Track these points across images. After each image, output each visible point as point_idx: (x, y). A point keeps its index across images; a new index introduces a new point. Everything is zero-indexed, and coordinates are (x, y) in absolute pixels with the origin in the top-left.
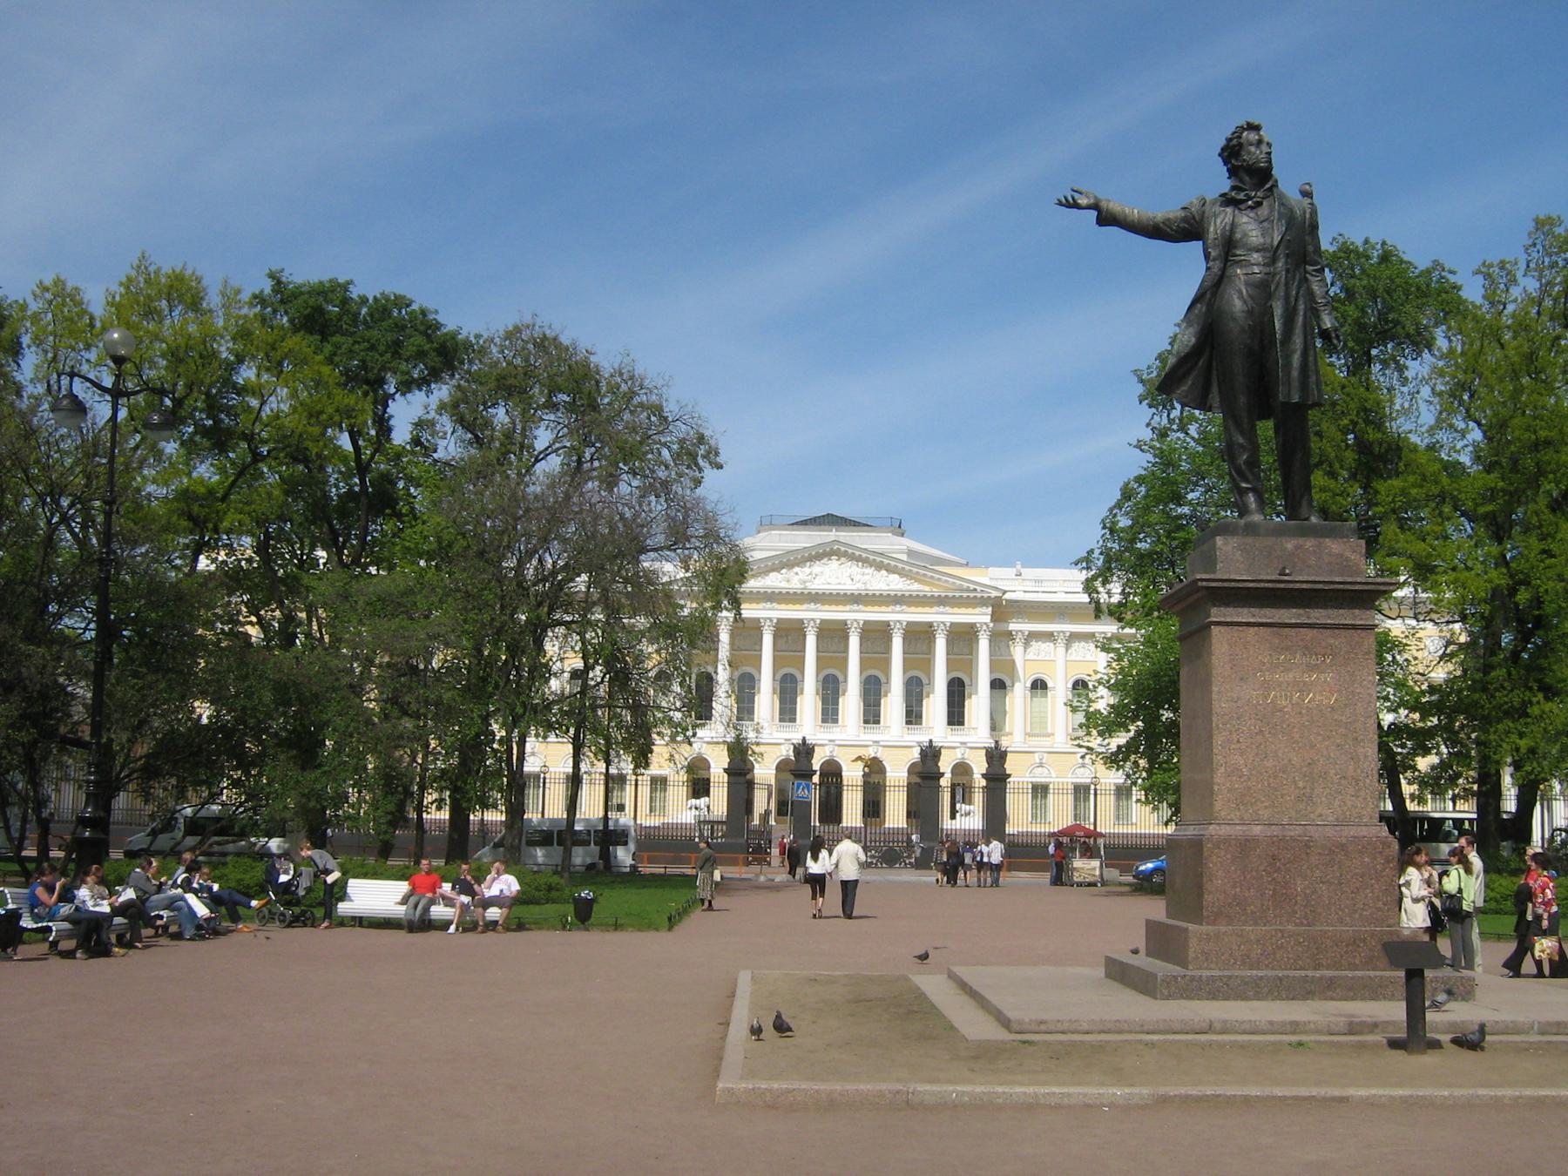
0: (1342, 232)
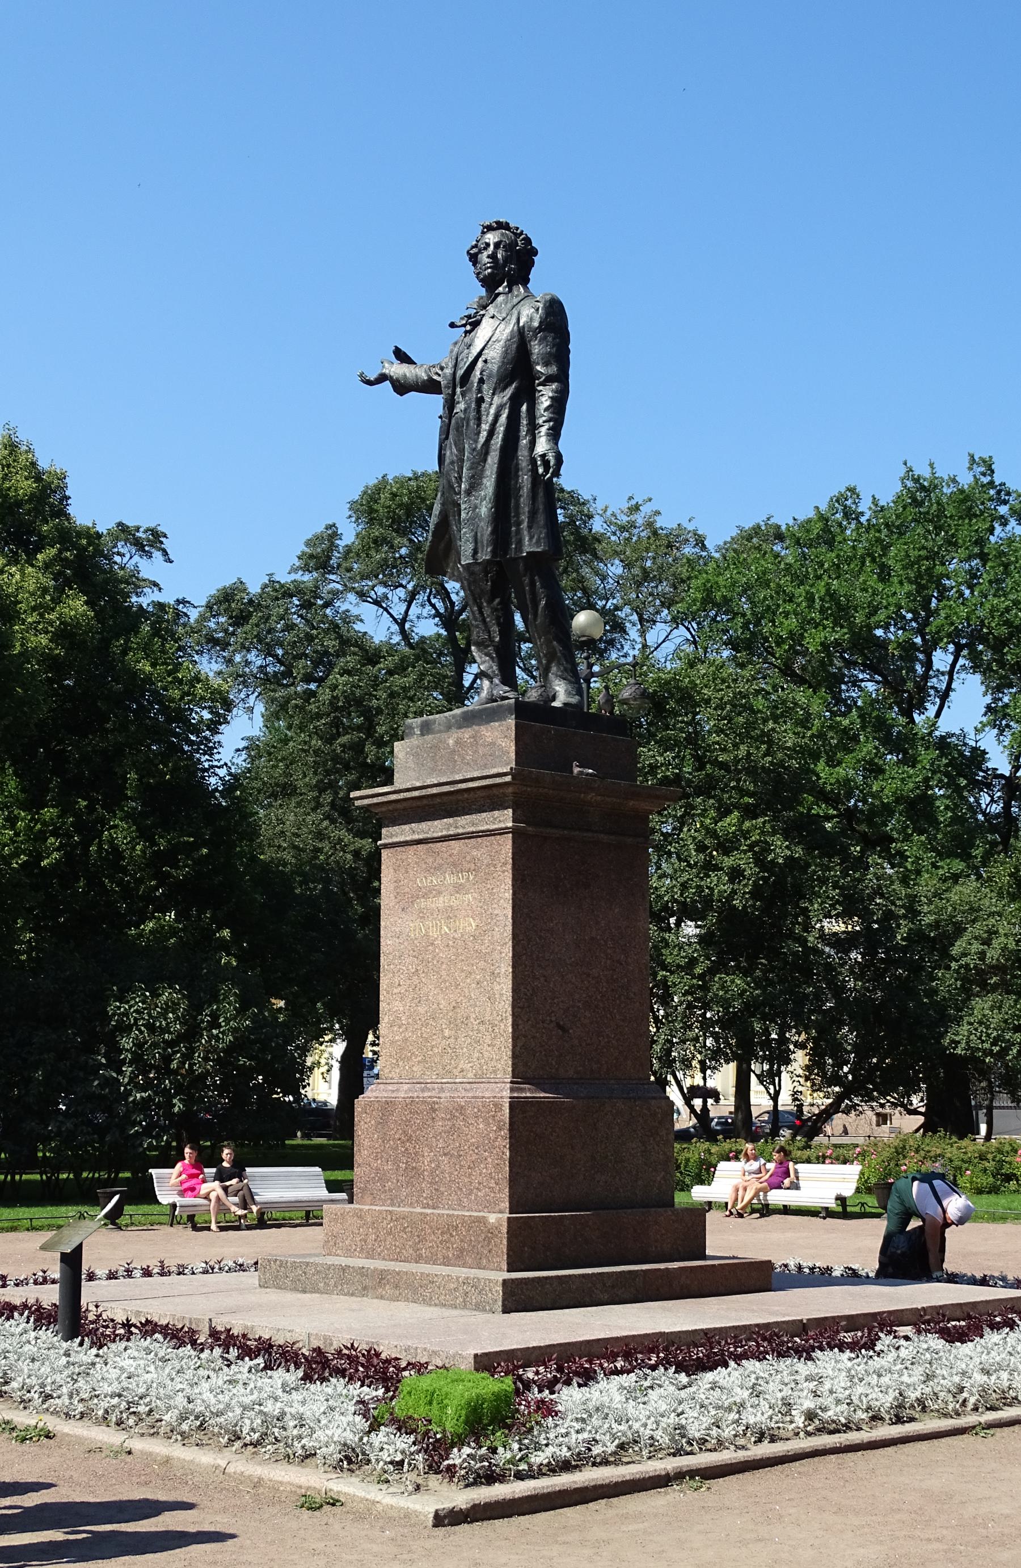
0: (454, 341)
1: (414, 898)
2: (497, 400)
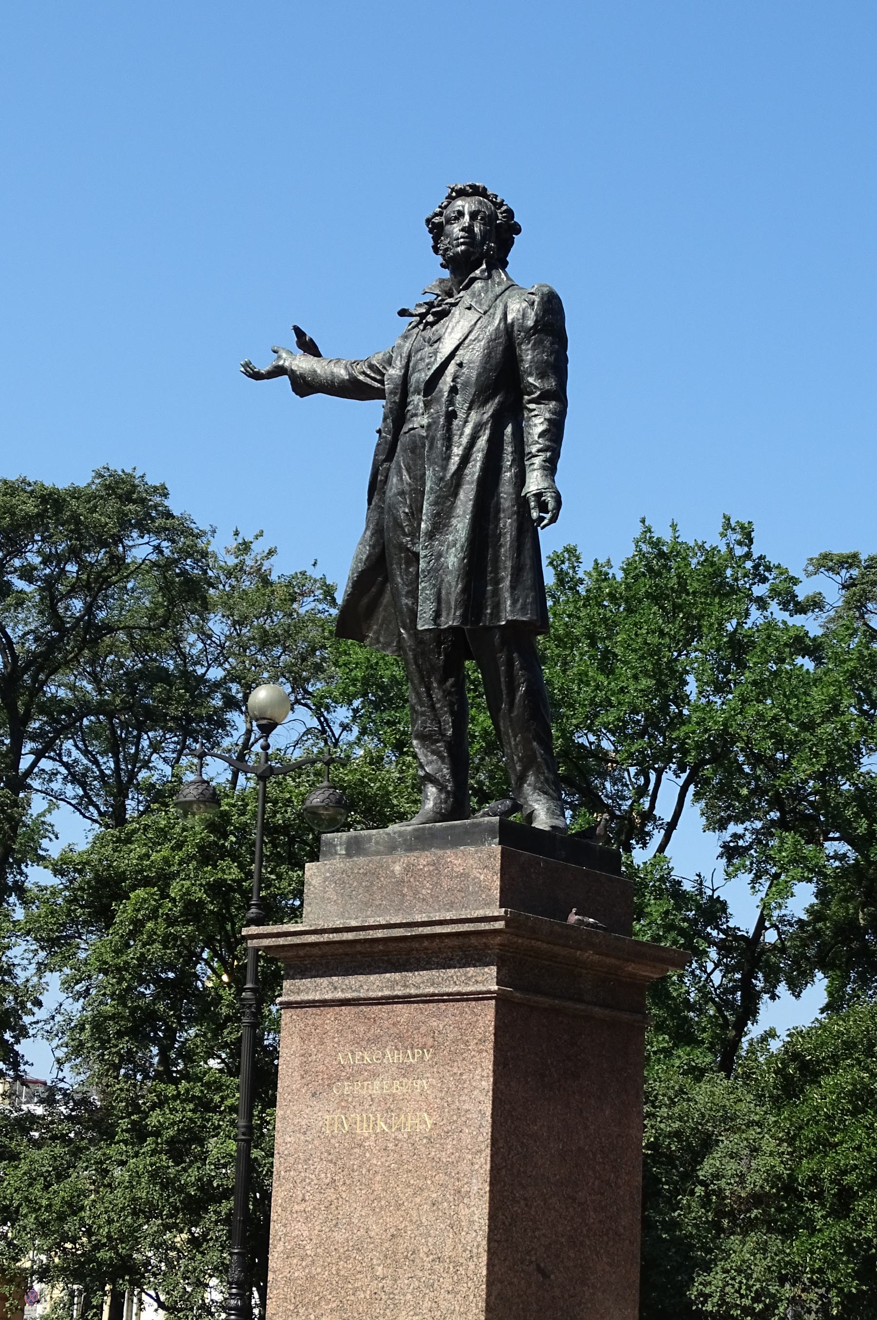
1: (332, 1080)
2: (474, 417)
